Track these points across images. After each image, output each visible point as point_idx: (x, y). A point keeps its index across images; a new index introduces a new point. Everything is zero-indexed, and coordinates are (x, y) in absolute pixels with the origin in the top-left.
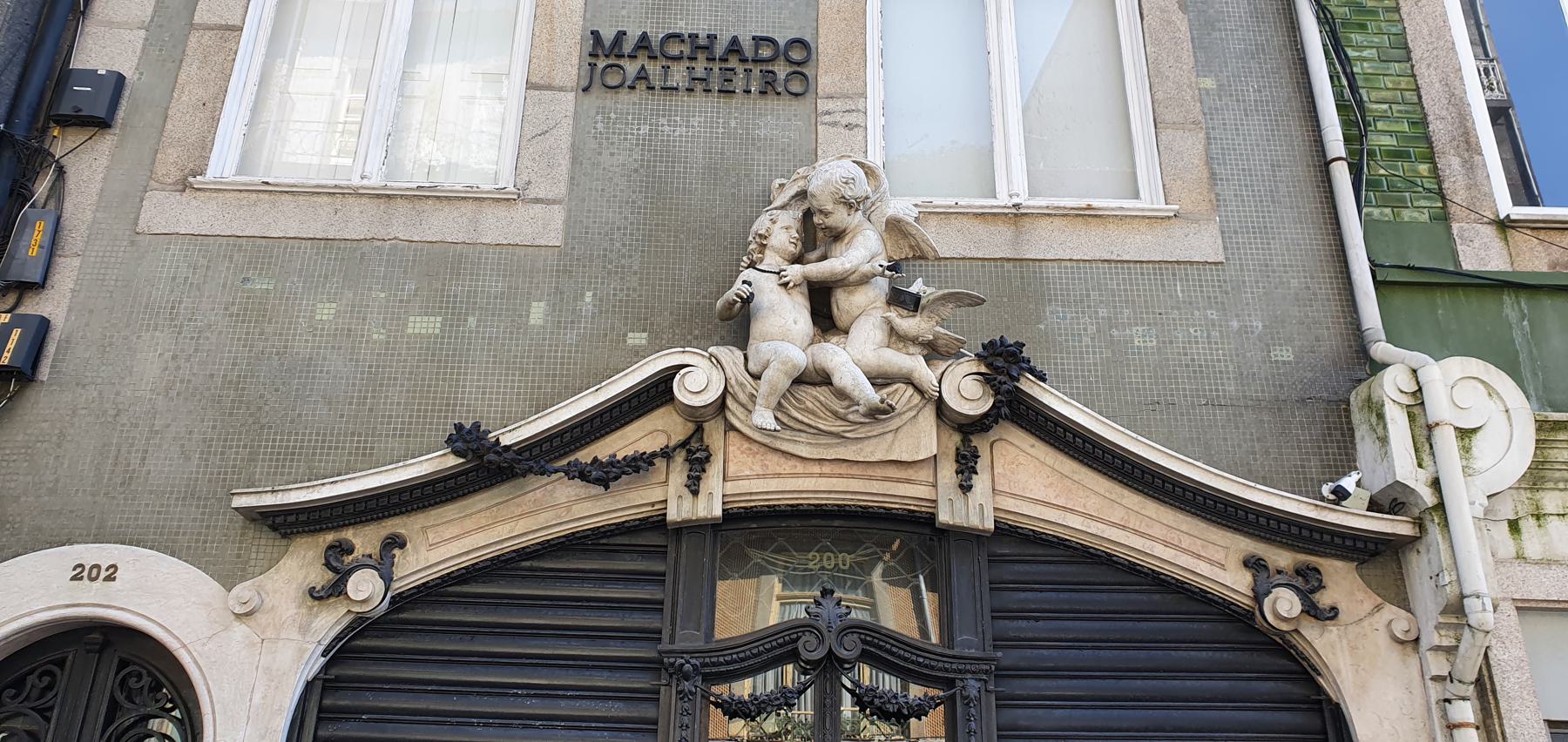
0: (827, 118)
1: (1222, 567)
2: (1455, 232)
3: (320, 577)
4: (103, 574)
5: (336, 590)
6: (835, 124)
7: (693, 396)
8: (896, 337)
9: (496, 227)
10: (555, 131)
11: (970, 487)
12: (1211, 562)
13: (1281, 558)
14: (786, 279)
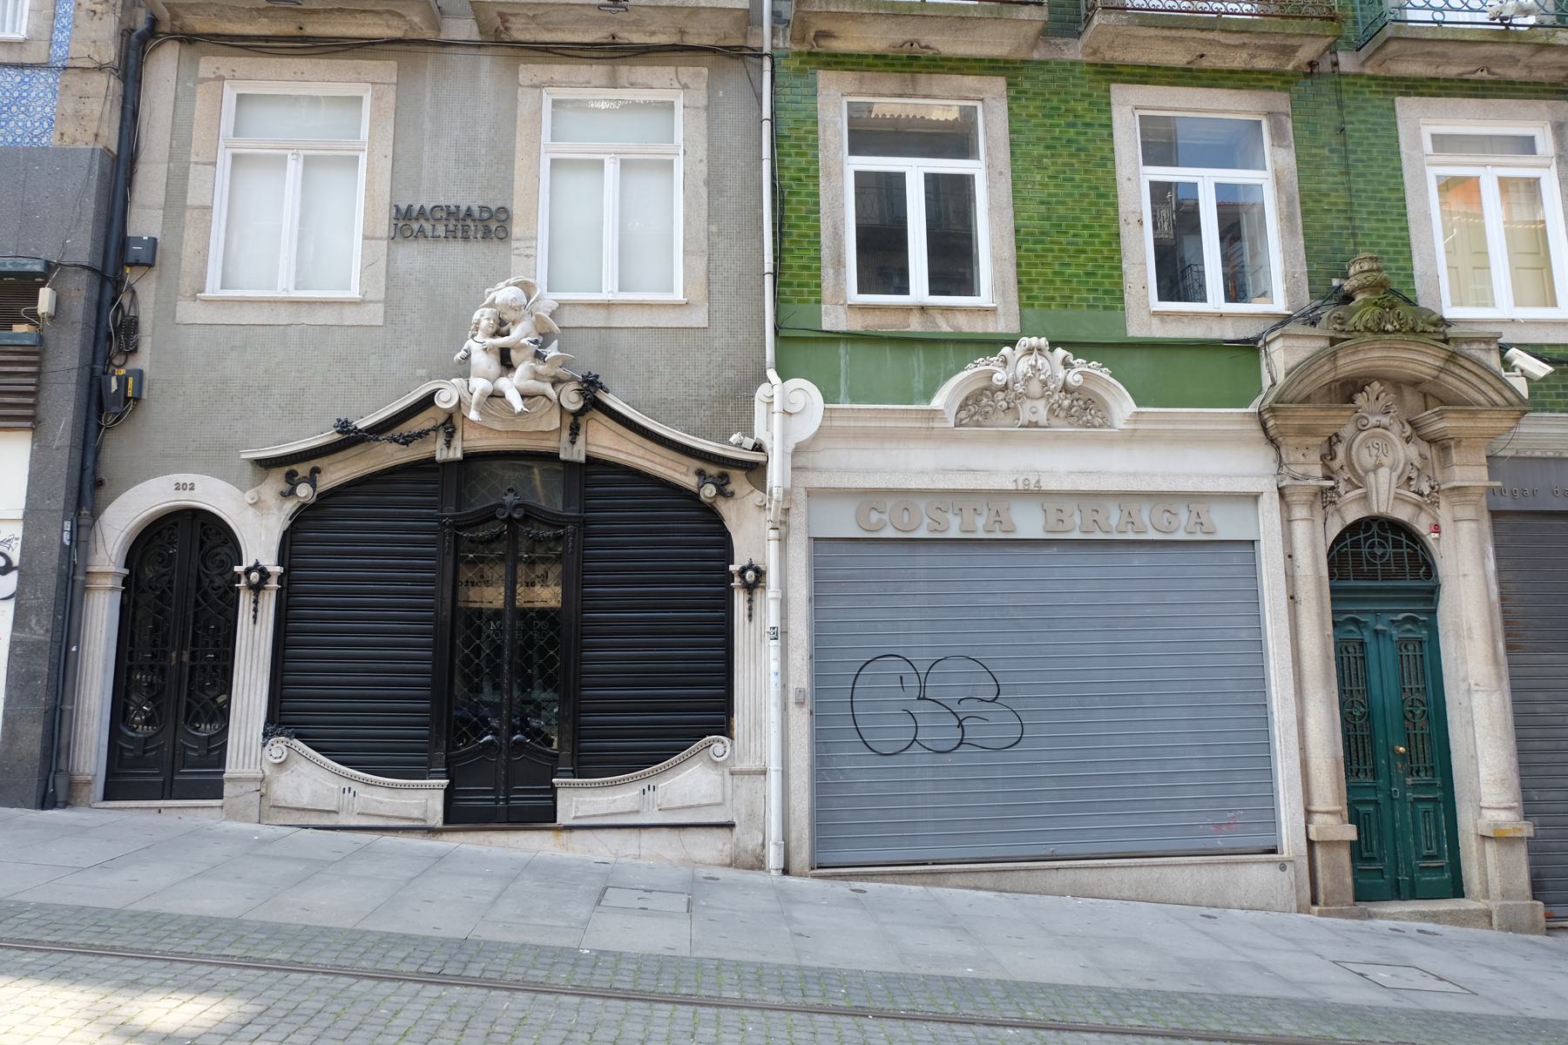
0: (517, 252)
1: (686, 475)
3: (285, 487)
6: (519, 255)
9: (350, 317)
13: (713, 470)
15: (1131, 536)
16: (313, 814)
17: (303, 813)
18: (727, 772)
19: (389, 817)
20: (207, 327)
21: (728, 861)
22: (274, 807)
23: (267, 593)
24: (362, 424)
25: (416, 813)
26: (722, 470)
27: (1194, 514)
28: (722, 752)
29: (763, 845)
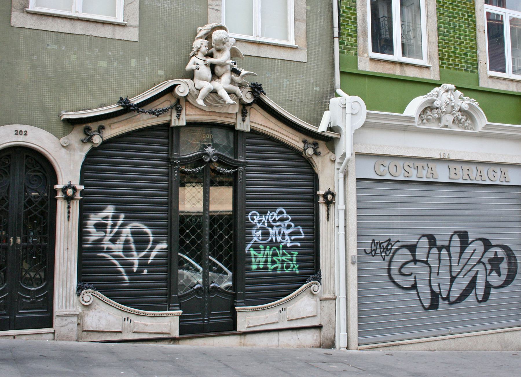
0: (211, 7)
1: (298, 142)
2: (358, 59)
3: (83, 137)
4: (24, 133)
5: (89, 140)
6: (213, 9)
7: (181, 94)
8: (232, 82)
9: (120, 34)
10: (134, 3)
11: (245, 120)
12: (295, 141)
13: (310, 140)
14: (207, 63)
15: (504, 183)
16: (108, 334)
17: (102, 334)
18: (318, 299)
19: (150, 333)
20: (31, 30)
21: (319, 345)
22: (85, 331)
23: (75, 202)
24: (135, 101)
25: (165, 330)
26: (315, 140)
27: (503, 173)
28: (317, 289)
29: (335, 335)
